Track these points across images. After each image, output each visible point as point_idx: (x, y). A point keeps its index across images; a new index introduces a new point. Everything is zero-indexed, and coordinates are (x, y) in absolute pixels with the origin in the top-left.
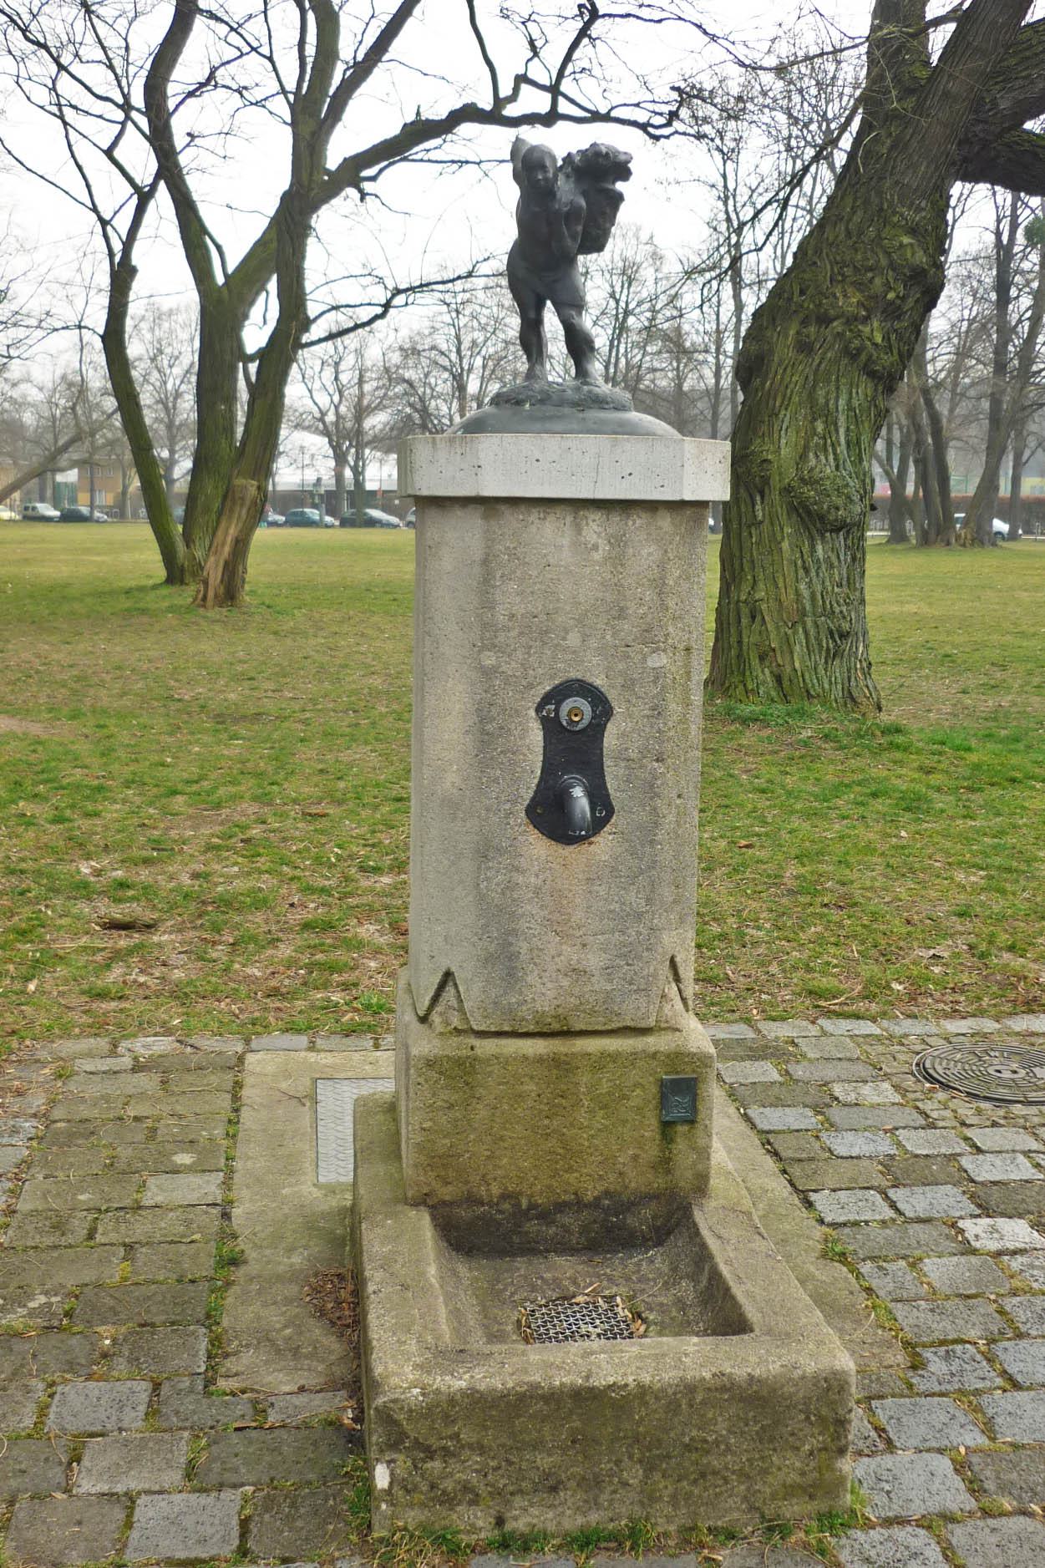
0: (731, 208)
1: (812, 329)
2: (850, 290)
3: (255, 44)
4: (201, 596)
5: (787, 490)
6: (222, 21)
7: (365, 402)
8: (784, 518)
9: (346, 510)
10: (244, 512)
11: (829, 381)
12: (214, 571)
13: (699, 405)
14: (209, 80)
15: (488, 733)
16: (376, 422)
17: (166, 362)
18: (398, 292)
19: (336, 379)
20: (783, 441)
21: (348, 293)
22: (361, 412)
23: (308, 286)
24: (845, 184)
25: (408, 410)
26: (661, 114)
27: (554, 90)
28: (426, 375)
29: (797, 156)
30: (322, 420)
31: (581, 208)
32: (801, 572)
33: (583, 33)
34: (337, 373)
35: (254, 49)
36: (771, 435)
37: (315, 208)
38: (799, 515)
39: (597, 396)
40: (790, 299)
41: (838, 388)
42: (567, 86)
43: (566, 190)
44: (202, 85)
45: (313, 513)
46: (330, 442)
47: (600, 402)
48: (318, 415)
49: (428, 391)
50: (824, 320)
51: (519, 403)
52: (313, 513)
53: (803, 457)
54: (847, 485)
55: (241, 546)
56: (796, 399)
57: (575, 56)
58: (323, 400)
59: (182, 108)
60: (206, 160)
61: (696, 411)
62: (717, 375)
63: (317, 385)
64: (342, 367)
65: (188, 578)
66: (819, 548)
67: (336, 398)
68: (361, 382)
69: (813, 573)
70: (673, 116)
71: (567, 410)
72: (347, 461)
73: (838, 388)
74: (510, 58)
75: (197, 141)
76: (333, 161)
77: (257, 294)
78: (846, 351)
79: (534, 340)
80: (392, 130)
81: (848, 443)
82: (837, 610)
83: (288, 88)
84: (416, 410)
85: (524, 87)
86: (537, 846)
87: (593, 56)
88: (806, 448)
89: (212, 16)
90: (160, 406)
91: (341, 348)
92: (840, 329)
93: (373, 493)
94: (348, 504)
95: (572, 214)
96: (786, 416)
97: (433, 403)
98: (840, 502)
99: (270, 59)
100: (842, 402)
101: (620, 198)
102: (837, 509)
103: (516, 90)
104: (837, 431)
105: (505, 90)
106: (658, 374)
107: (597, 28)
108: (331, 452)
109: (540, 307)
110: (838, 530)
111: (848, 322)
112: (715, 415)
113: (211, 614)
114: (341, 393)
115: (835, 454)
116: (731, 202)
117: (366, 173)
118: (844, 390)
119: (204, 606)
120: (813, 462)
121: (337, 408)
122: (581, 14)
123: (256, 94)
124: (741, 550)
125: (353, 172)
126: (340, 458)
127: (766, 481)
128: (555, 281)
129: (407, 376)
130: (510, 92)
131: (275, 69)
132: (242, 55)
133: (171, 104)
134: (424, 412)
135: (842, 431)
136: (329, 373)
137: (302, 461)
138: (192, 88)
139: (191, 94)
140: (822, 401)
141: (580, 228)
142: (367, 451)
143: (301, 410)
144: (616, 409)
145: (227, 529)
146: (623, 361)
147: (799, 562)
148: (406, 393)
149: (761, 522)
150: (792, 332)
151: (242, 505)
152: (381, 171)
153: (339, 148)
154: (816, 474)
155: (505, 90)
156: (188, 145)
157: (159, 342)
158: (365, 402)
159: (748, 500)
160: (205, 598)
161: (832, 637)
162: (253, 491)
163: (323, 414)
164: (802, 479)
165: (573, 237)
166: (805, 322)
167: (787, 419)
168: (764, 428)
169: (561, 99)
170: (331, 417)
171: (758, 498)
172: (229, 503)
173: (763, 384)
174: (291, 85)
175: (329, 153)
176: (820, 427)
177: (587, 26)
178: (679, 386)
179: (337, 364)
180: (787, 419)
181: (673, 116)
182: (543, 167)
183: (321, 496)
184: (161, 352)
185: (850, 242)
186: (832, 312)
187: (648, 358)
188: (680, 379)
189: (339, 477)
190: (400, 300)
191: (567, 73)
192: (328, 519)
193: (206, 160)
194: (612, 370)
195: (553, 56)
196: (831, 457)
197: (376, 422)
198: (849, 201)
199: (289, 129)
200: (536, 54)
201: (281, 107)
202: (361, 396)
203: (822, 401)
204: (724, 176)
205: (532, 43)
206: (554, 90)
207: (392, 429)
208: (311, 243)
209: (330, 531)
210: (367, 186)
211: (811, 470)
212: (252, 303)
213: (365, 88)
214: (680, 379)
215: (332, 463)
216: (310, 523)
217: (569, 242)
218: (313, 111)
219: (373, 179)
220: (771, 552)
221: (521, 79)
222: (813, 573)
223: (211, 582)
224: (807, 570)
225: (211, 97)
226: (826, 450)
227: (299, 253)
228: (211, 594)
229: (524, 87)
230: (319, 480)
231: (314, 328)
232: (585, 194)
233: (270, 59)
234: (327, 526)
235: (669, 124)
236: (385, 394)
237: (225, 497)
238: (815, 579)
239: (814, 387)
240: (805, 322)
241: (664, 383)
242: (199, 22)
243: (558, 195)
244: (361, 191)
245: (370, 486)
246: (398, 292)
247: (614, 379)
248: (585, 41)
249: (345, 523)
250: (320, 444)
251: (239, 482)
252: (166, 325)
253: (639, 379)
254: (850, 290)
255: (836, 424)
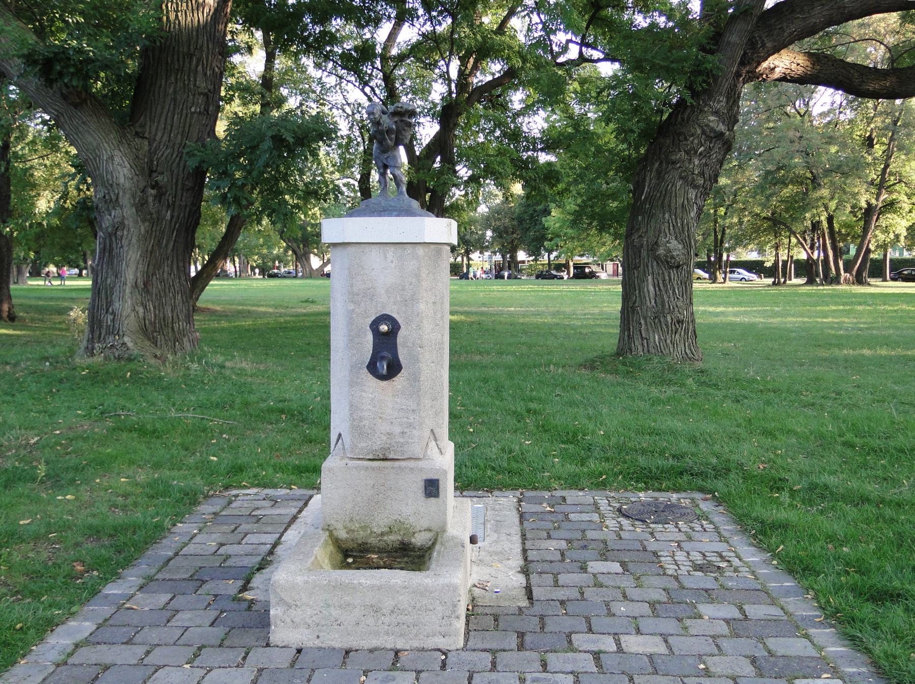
15: (353, 340)
86: (372, 382)
141: (393, 136)
165: (391, 140)
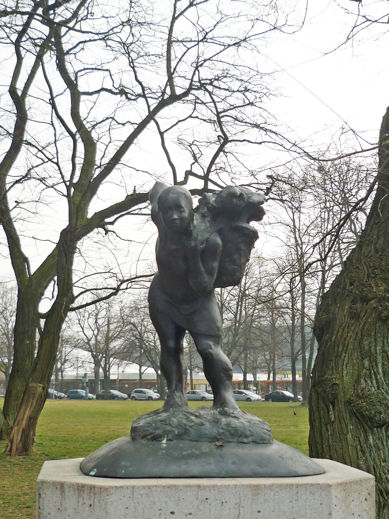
0: (297, 236)
1: (359, 305)
2: (379, 282)
3: (51, 157)
4: (8, 449)
5: (349, 402)
6: (34, 146)
7: (110, 335)
8: (348, 420)
9: (100, 391)
10: (34, 402)
11: (370, 335)
12: (17, 435)
13: (284, 334)
14: (27, 175)
16: (116, 344)
17: (8, 314)
18: (123, 282)
19: (96, 322)
20: (345, 372)
21: (90, 283)
22: (108, 340)
23: (75, 279)
24: (372, 223)
25: (133, 338)
26: (262, 190)
27: (206, 178)
28: (142, 321)
29: (330, 211)
30: (88, 343)
31: (217, 244)
32: (360, 453)
33: (221, 149)
34: (96, 319)
35: (50, 160)
36: (337, 368)
37: (79, 239)
38: (357, 417)
39: (236, 429)
40: (344, 288)
41: (376, 340)
42: (212, 176)
43: (201, 227)
44: (24, 177)
45: (82, 392)
46: (92, 355)
47: (238, 436)
48: (86, 341)
49: (143, 328)
50: (365, 300)
51: (156, 438)
52: (82, 392)
53: (358, 382)
54: (385, 398)
55: (32, 421)
56: (351, 347)
57: (217, 161)
58: (89, 333)
59: (12, 189)
60: (25, 215)
61: (283, 338)
62: (293, 319)
63: (86, 325)
64: (99, 317)
65: (5, 436)
66: (371, 438)
67: (96, 332)
68: (109, 324)
69: (368, 454)
70: (269, 190)
71: (206, 447)
72: (100, 365)
73: (376, 340)
74: (183, 162)
75: (21, 205)
76: (90, 214)
77: (49, 282)
78: (379, 318)
79: (174, 367)
80: (121, 198)
81: (384, 372)
82: (384, 477)
83: (66, 179)
84: (137, 338)
85: (191, 178)
87: (226, 161)
88: (359, 376)
89: (30, 144)
90: (5, 336)
91: (99, 307)
92: (375, 305)
93: (114, 381)
94: (101, 387)
95: (208, 252)
96: (345, 357)
97: (146, 335)
98: (382, 409)
99: (57, 164)
100: (378, 348)
101: (253, 236)
102: (380, 413)
103: (186, 179)
104: (377, 366)
105: (180, 178)
106: (262, 319)
107: (228, 147)
108: (92, 360)
109: (179, 336)
110: (381, 426)
111: (379, 301)
112: (293, 341)
113: (13, 460)
114: (98, 330)
115: (376, 379)
116: (297, 233)
117: (107, 220)
118: (379, 340)
119: (10, 455)
120: (364, 385)
121: (96, 337)
122: (219, 140)
123: (50, 182)
124: (322, 439)
125: (100, 220)
126: (97, 363)
127: (335, 397)
128: (194, 313)
129: (132, 320)
130: (183, 179)
131: (60, 169)
132: (44, 162)
133: (8, 187)
134: (141, 339)
135: (380, 365)
136: (92, 321)
137: (76, 364)
138: (18, 178)
139: (17, 182)
140: (367, 347)
141: (216, 265)
142: (111, 359)
143: (78, 338)
144: (255, 442)
145: (26, 410)
146: (244, 312)
147: (359, 447)
148: (131, 330)
149: (333, 422)
150: (346, 307)
151: (34, 398)
152: (117, 219)
153: (95, 206)
154: (366, 392)
155: (180, 178)
156: (15, 207)
157: (6, 304)
158: (110, 335)
159: (325, 409)
160: (11, 450)
161: (382, 494)
162: (40, 390)
163: (89, 340)
164: (358, 396)
165: (210, 273)
166: (354, 302)
167: (346, 359)
168: (333, 364)
169: (209, 183)
170: (93, 342)
171: (331, 407)
172: (26, 397)
173: (331, 338)
174: (67, 178)
175: (89, 211)
176: (367, 363)
177: (222, 146)
178: (273, 324)
179: (97, 315)
180: (346, 359)
181: (269, 190)
182: (179, 208)
183: (87, 383)
184: (6, 308)
185: (377, 255)
186: (369, 295)
187: (257, 311)
188: (273, 322)
189: (96, 373)
190: (124, 286)
191: (212, 170)
192: (90, 395)
193: (25, 215)
194: (238, 317)
195: (205, 162)
196: (374, 381)
197: (116, 344)
198: (375, 232)
199: (66, 199)
200: (196, 160)
201: (62, 188)
202: (109, 331)
203: (367, 347)
204: (293, 221)
205: (194, 156)
206: (206, 178)
207: (124, 348)
208: (77, 258)
209: (90, 402)
210: (109, 227)
211: (363, 390)
212: (46, 287)
213: (108, 178)
214: (273, 322)
215: (93, 366)
216: (81, 398)
217: (206, 278)
218: (81, 190)
219: (112, 223)
220: (341, 441)
221: (189, 173)
222: (368, 454)
223: (15, 441)
224: (363, 452)
225: (27, 183)
226: (371, 377)
227: (70, 262)
228: (14, 448)
229: (191, 178)
230: (86, 374)
231: (76, 300)
232: (220, 232)
233: (57, 164)
234: (90, 399)
235: (267, 194)
236: (121, 330)
237: (25, 393)
238: (369, 458)
239: (362, 339)
240: (354, 302)
241: (265, 323)
242: (24, 148)
243: (194, 234)
244: (105, 230)
245: (112, 377)
246: (123, 282)
247: (239, 321)
248: (222, 153)
249: (99, 397)
250: (86, 355)
251: (34, 384)
252: (10, 295)
253: (252, 321)
254: (379, 282)
255: (376, 361)
